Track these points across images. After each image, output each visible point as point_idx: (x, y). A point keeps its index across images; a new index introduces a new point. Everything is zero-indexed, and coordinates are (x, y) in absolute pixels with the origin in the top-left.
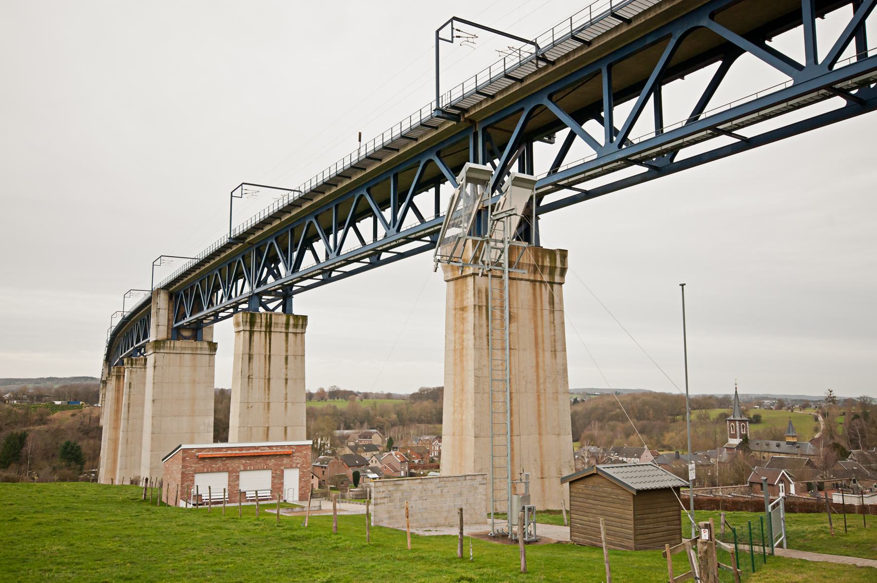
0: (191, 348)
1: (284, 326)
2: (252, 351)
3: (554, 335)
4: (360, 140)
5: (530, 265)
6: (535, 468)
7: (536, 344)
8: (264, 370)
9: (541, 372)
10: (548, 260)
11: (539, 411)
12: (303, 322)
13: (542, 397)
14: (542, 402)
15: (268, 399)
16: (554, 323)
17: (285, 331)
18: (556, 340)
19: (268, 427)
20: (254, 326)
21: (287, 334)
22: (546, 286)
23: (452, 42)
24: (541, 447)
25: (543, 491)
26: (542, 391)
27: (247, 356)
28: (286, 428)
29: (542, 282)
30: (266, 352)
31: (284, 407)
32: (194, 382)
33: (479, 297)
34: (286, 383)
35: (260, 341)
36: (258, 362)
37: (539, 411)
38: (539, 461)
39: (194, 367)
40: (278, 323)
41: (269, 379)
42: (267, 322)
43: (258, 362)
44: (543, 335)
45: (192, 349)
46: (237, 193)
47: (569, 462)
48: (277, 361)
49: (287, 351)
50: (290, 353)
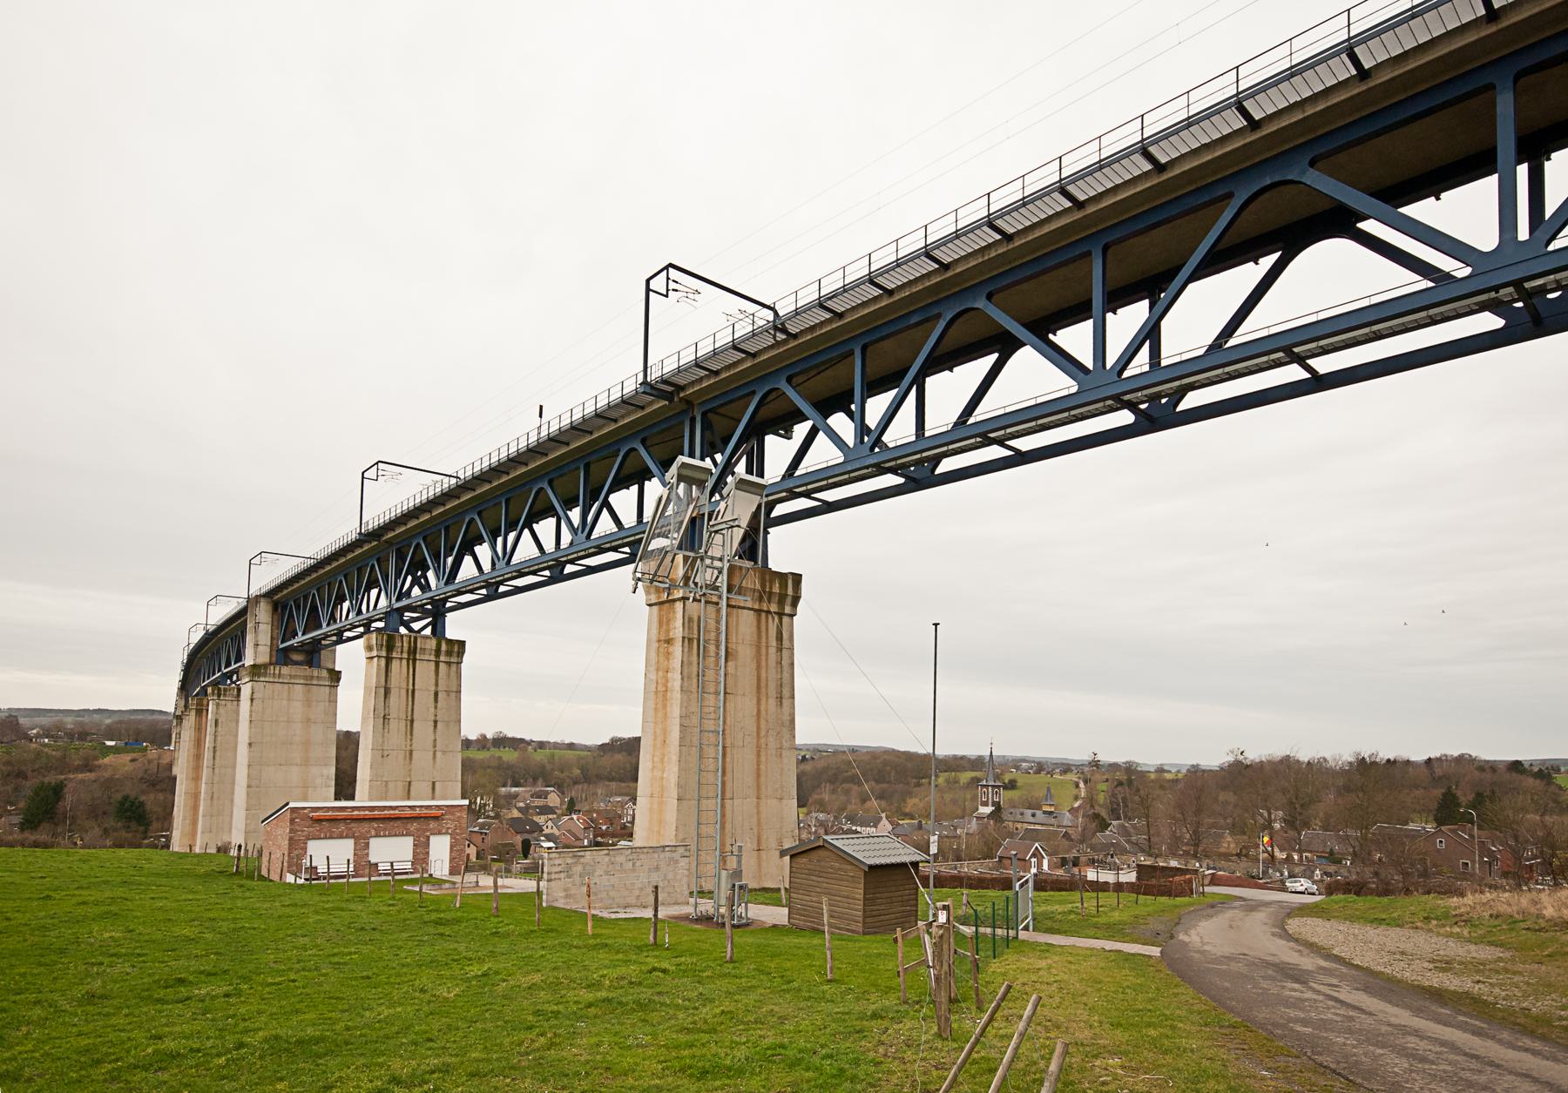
4: (541, 416)
5: (754, 590)
7: (759, 688)
9: (763, 722)
11: (758, 769)
13: (763, 753)
14: (763, 759)
19: (410, 782)
21: (437, 664)
23: (667, 296)
24: (758, 813)
28: (434, 783)
31: (432, 756)
32: (308, 721)
34: (435, 726)
36: (397, 700)
37: (758, 769)
38: (755, 831)
39: (308, 702)
42: (410, 647)
43: (397, 700)
45: (305, 678)
46: (371, 474)
48: (424, 698)
49: (437, 685)
50: (440, 688)
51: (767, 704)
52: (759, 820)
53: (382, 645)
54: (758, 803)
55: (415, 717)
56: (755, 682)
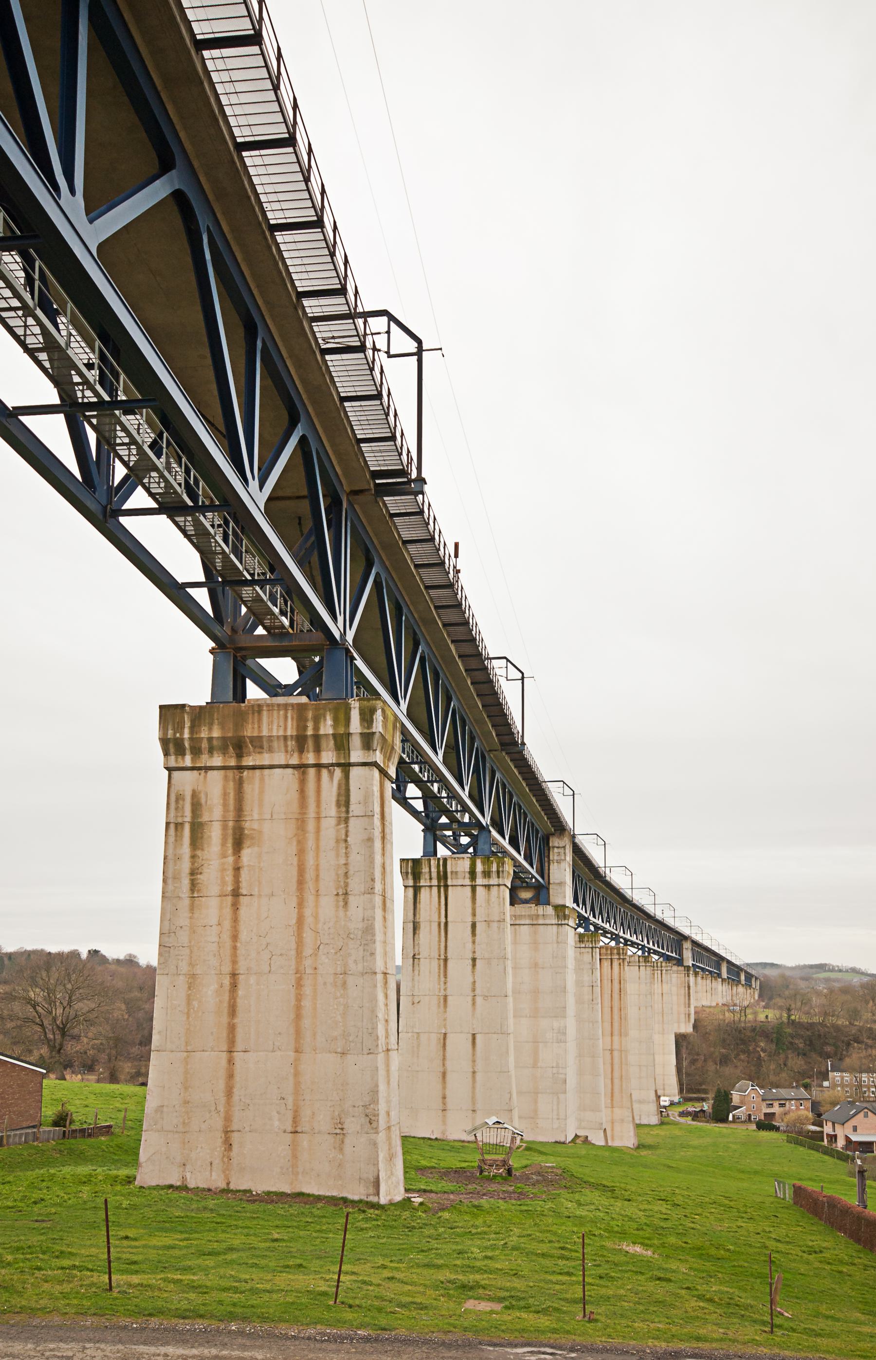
0: (529, 916)
1: (467, 875)
2: (418, 916)
3: (346, 864)
5: (285, 738)
6: (278, 1113)
8: (437, 947)
9: (308, 936)
10: (329, 722)
11: (298, 1008)
12: (498, 867)
13: (307, 982)
14: (307, 990)
15: (445, 990)
16: (346, 841)
17: (469, 883)
18: (351, 873)
19: (445, 1034)
20: (420, 880)
21: (474, 888)
22: (331, 774)
24: (297, 1074)
25: (295, 1157)
26: (309, 971)
27: (411, 925)
28: (474, 1035)
29: (318, 766)
30: (439, 917)
31: (470, 1002)
33: (177, 809)
34: (474, 965)
35: (431, 901)
36: (428, 935)
37: (298, 1008)
38: (290, 1101)
39: (535, 944)
40: (456, 873)
41: (446, 960)
42: (438, 872)
43: (428, 935)
44: (317, 868)
45: (531, 917)
47: (364, 1106)
48: (459, 932)
49: (474, 915)
50: (478, 918)
51: (317, 906)
52: (297, 1084)
53: (407, 873)
54: (297, 1060)
55: (449, 955)
56: (294, 872)
